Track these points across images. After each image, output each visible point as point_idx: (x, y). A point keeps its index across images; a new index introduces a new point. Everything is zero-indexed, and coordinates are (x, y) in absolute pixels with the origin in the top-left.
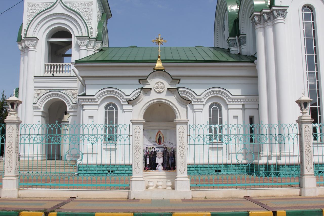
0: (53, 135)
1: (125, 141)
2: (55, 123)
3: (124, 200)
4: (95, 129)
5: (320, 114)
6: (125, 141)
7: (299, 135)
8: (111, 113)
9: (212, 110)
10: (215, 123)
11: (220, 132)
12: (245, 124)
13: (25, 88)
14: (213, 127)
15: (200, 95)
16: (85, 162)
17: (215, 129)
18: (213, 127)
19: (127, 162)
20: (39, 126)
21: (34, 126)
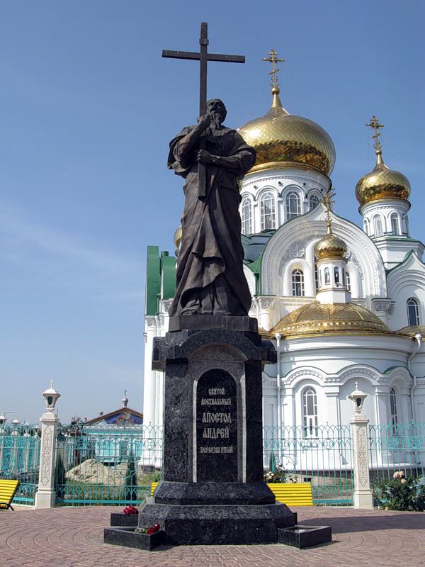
10: (311, 413)
11: (316, 424)
14: (308, 417)
18: (308, 417)
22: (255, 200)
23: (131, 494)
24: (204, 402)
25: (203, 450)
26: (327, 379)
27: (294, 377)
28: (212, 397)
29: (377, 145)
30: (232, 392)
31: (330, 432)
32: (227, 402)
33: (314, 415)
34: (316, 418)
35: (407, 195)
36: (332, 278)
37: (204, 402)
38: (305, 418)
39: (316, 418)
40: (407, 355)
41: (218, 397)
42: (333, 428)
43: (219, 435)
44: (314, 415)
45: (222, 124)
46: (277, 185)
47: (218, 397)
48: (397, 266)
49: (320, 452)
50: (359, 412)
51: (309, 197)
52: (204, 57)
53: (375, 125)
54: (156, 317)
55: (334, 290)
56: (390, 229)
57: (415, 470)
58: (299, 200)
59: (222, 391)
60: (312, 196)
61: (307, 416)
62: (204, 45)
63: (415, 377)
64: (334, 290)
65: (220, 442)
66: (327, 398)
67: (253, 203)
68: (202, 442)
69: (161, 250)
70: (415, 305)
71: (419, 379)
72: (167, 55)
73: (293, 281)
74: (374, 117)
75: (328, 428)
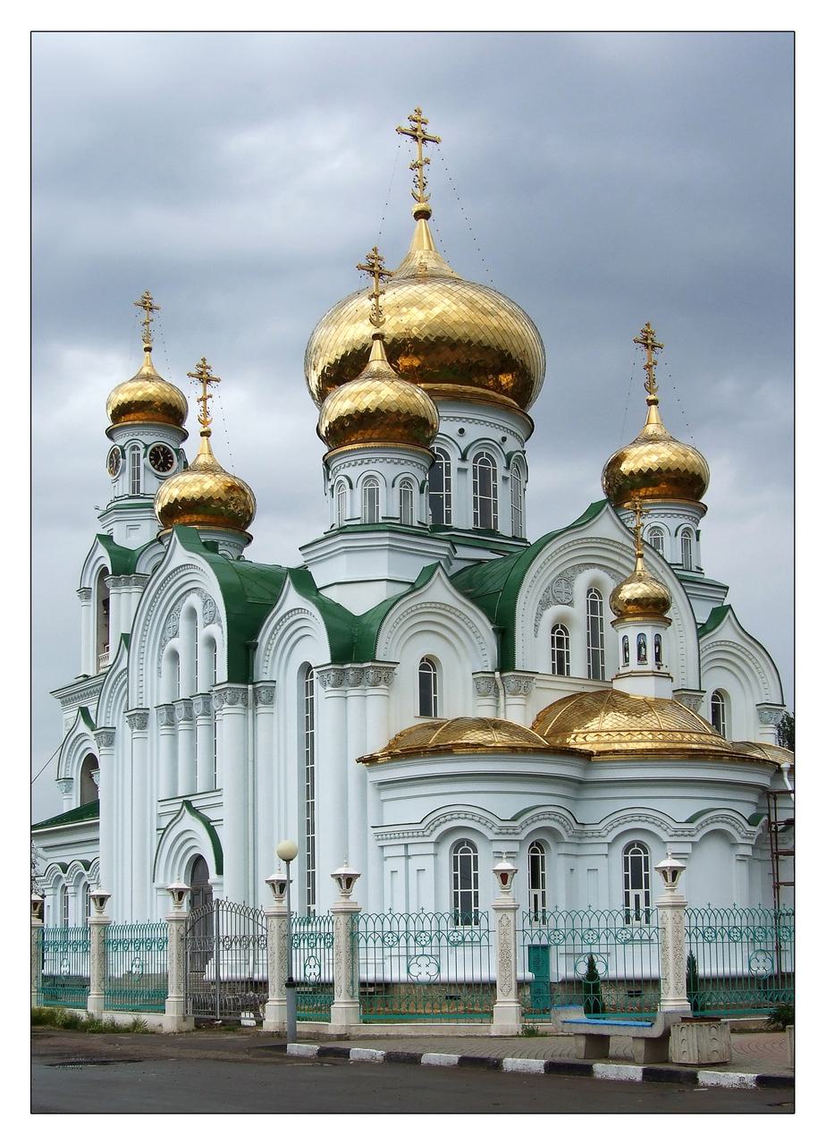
1: (367, 941)
4: (395, 921)
5: (456, 876)
6: (367, 941)
8: (636, 862)
9: (629, 856)
10: (637, 885)
11: (647, 904)
12: (41, 916)
13: (282, 775)
14: (633, 893)
15: (577, 823)
17: (637, 897)
18: (633, 893)
19: (485, 977)
20: (447, 916)
23: (592, 1004)
26: (501, 828)
27: (436, 823)
29: (650, 386)
31: (594, 919)
33: (644, 890)
38: (627, 894)
39: (543, 893)
42: (430, 916)
44: (644, 890)
50: (673, 890)
51: (470, 456)
53: (648, 343)
58: (495, 471)
61: (630, 890)
66: (738, 863)
74: (648, 325)
75: (590, 914)
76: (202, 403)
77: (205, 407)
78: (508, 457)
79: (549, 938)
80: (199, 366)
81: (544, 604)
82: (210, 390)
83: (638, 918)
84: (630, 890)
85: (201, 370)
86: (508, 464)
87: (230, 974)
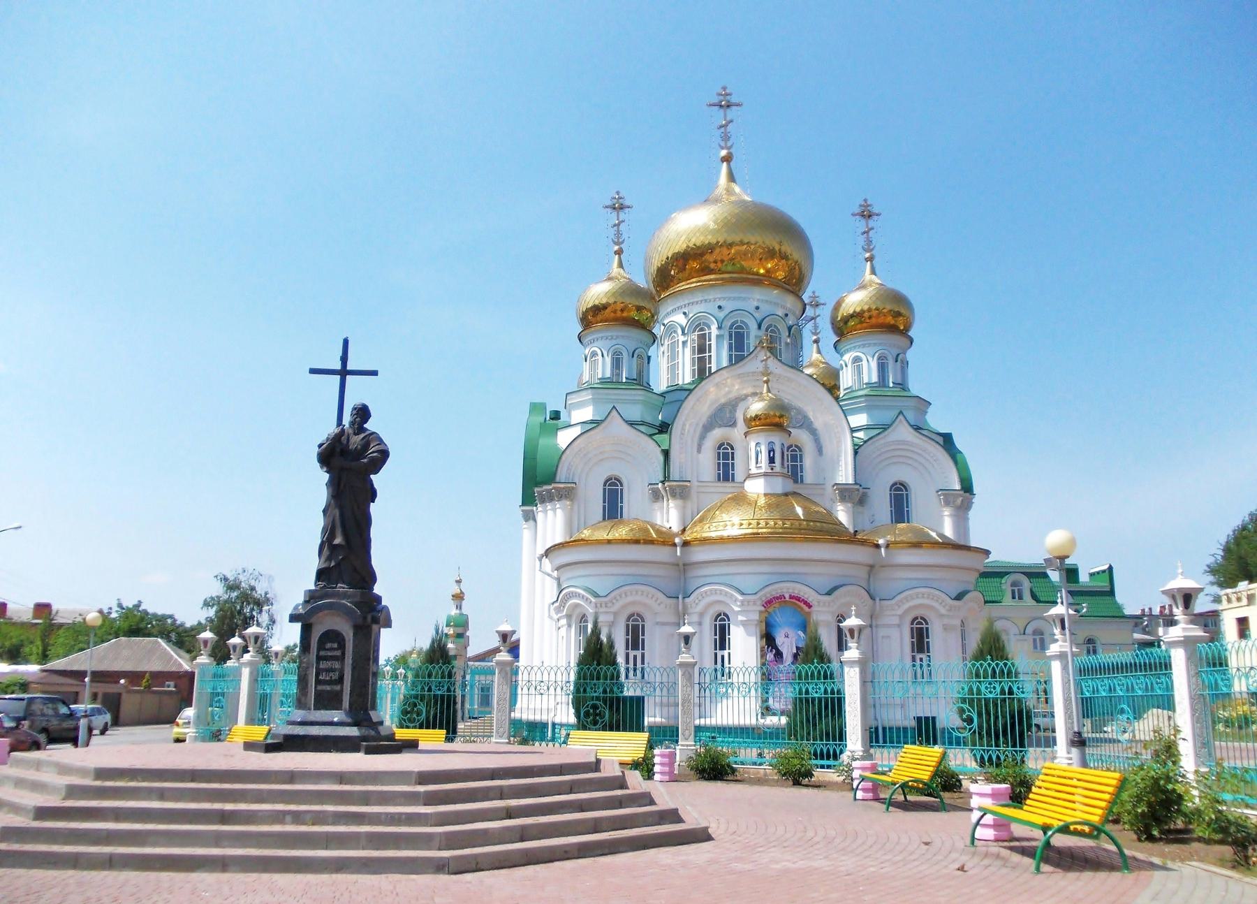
0: (983, 682)
1: (635, 691)
2: (985, 660)
3: (89, 782)
6: (635, 691)
7: (1032, 725)
8: (920, 631)
10: (635, 647)
11: (643, 663)
14: (632, 653)
16: (348, 707)
17: (635, 657)
18: (720, 653)
20: (755, 669)
21: (535, 669)
22: (683, 333)
24: (322, 653)
25: (320, 688)
28: (328, 650)
30: (342, 647)
32: (338, 653)
33: (641, 651)
34: (729, 654)
35: (908, 327)
36: (764, 457)
37: (322, 653)
38: (716, 654)
39: (729, 654)
40: (869, 568)
41: (332, 649)
43: (331, 677)
44: (641, 651)
45: (365, 426)
46: (715, 311)
47: (332, 649)
48: (879, 434)
49: (736, 700)
51: (764, 326)
52: (344, 373)
53: (866, 214)
54: (535, 508)
55: (765, 475)
56: (875, 379)
57: (900, 728)
59: (335, 645)
60: (770, 326)
62: (344, 359)
63: (877, 600)
64: (765, 475)
65: (330, 682)
67: (682, 338)
68: (318, 682)
69: (550, 408)
70: (904, 492)
71: (883, 602)
72: (313, 371)
73: (719, 459)
76: (616, 228)
77: (868, 238)
78: (790, 328)
79: (642, 689)
80: (861, 206)
81: (708, 428)
82: (871, 223)
83: (635, 675)
84: (718, 651)
85: (863, 208)
86: (790, 334)
87: (1156, 723)
